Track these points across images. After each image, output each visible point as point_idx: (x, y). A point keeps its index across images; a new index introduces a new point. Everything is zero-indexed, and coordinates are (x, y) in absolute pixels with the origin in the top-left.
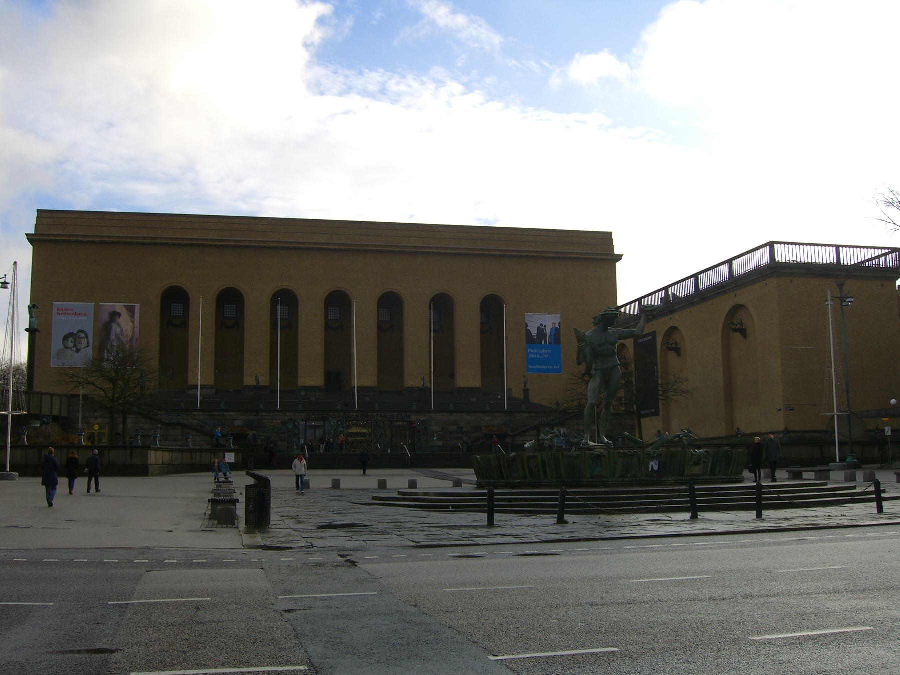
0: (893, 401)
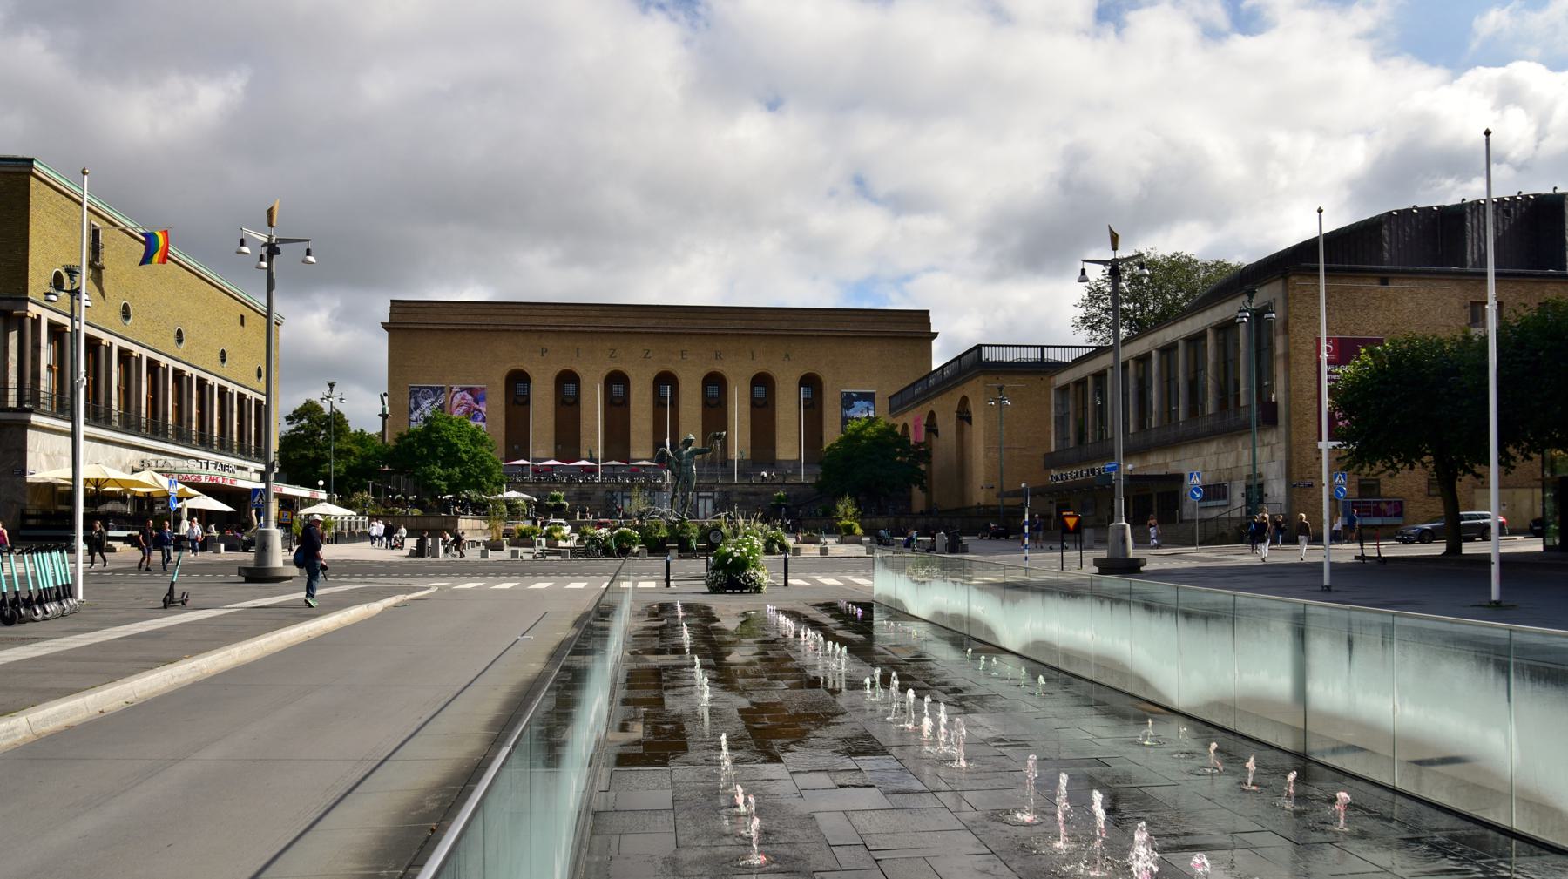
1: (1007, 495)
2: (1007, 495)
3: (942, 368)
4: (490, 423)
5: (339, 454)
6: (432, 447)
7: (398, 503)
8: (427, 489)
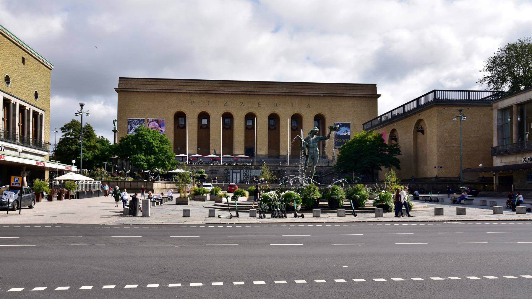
0: (480, 165)
4: (168, 132)
5: (89, 148)
6: (139, 144)
7: (121, 174)
8: (136, 167)
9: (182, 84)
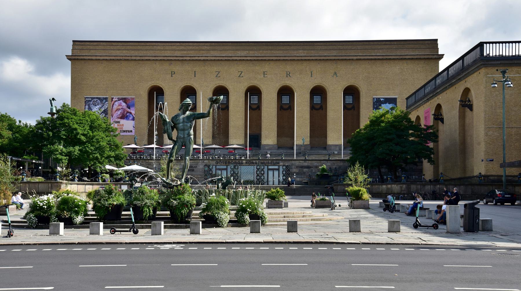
1: (512, 165)
2: (512, 165)
3: (447, 69)
9: (159, 48)
